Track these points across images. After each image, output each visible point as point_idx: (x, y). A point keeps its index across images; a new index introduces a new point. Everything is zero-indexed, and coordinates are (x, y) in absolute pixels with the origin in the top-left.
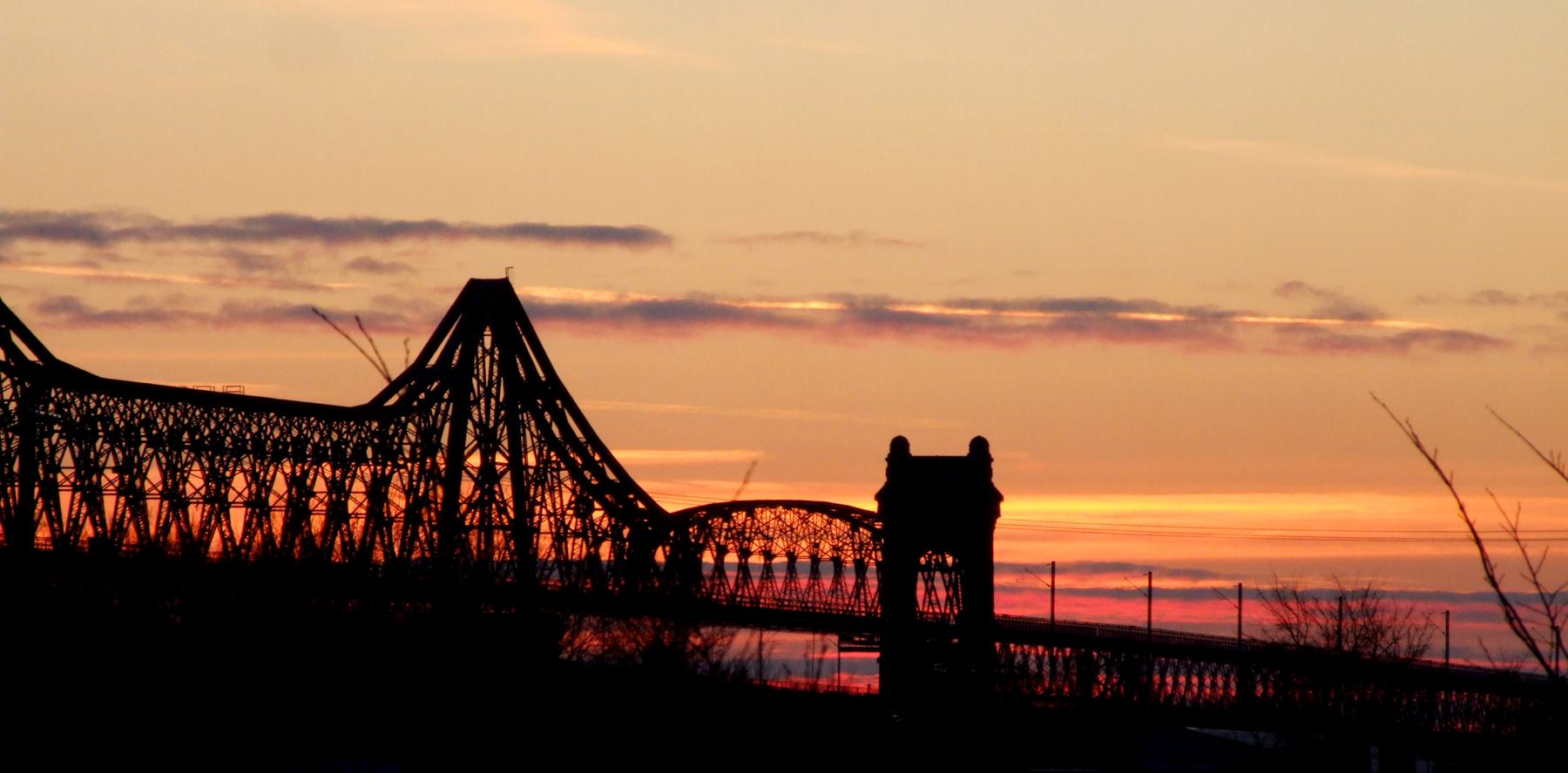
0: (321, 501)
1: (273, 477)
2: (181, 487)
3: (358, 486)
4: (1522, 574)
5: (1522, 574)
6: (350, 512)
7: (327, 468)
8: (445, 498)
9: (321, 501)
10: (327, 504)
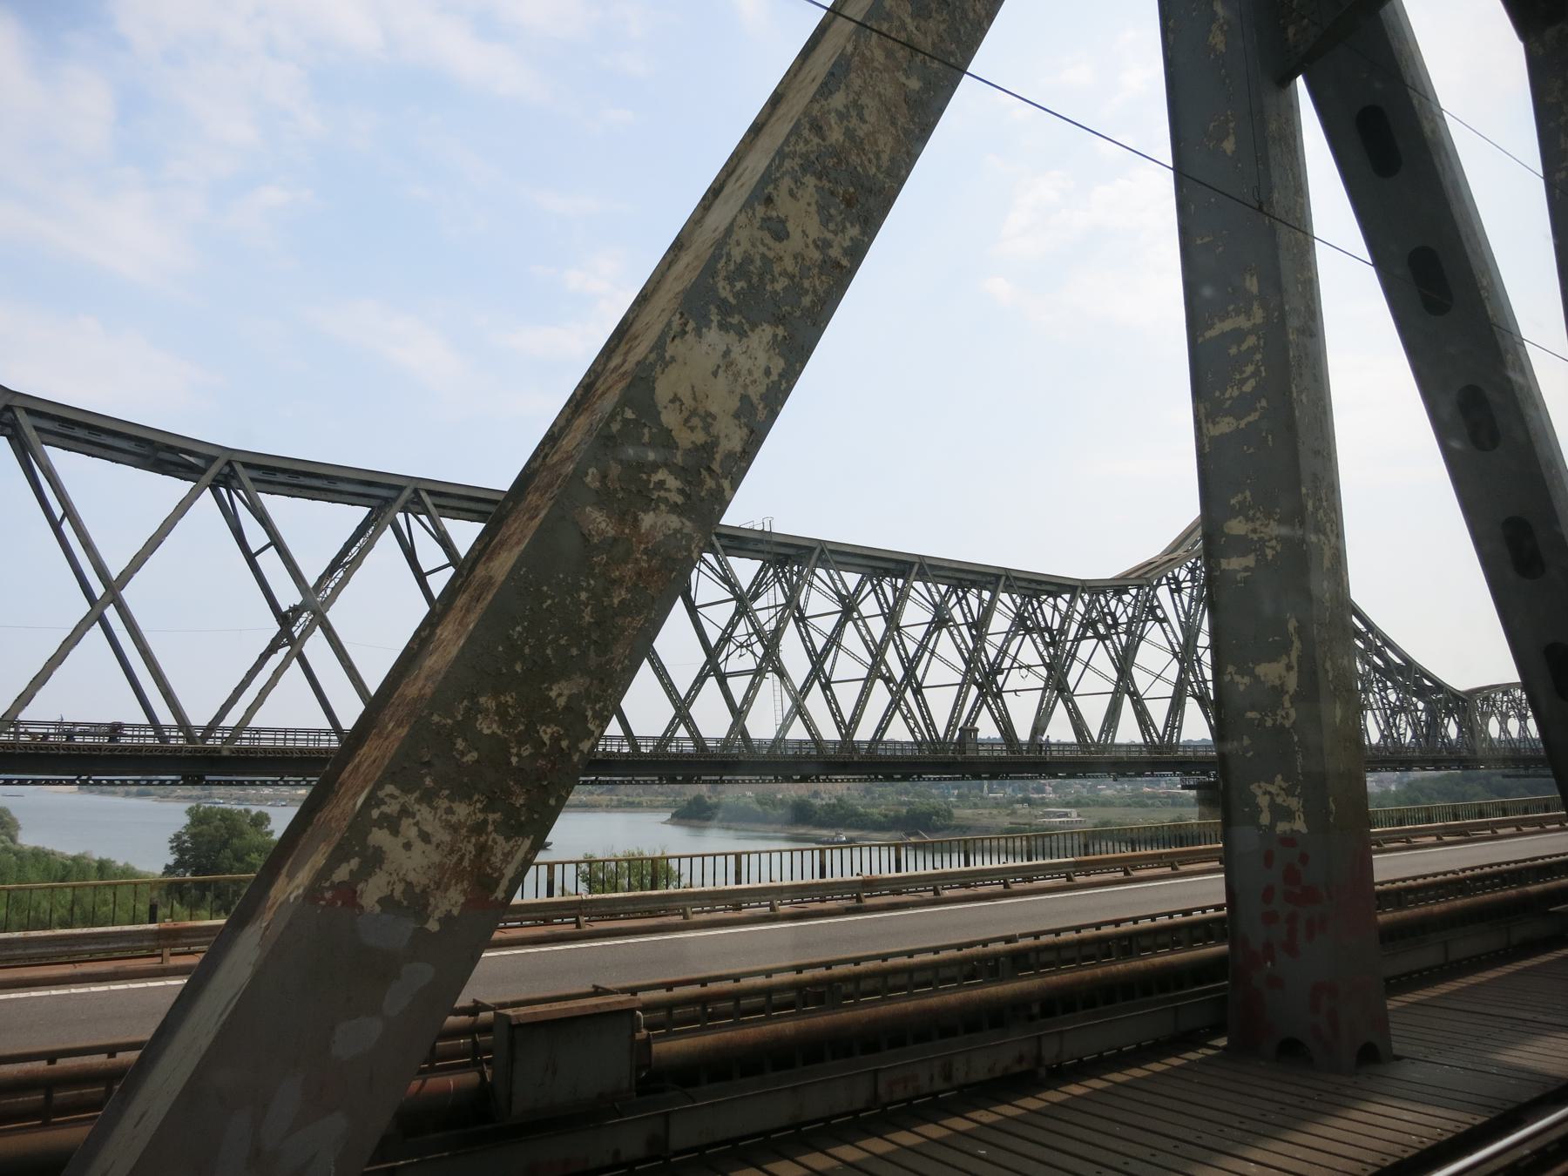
6: (1209, 650)
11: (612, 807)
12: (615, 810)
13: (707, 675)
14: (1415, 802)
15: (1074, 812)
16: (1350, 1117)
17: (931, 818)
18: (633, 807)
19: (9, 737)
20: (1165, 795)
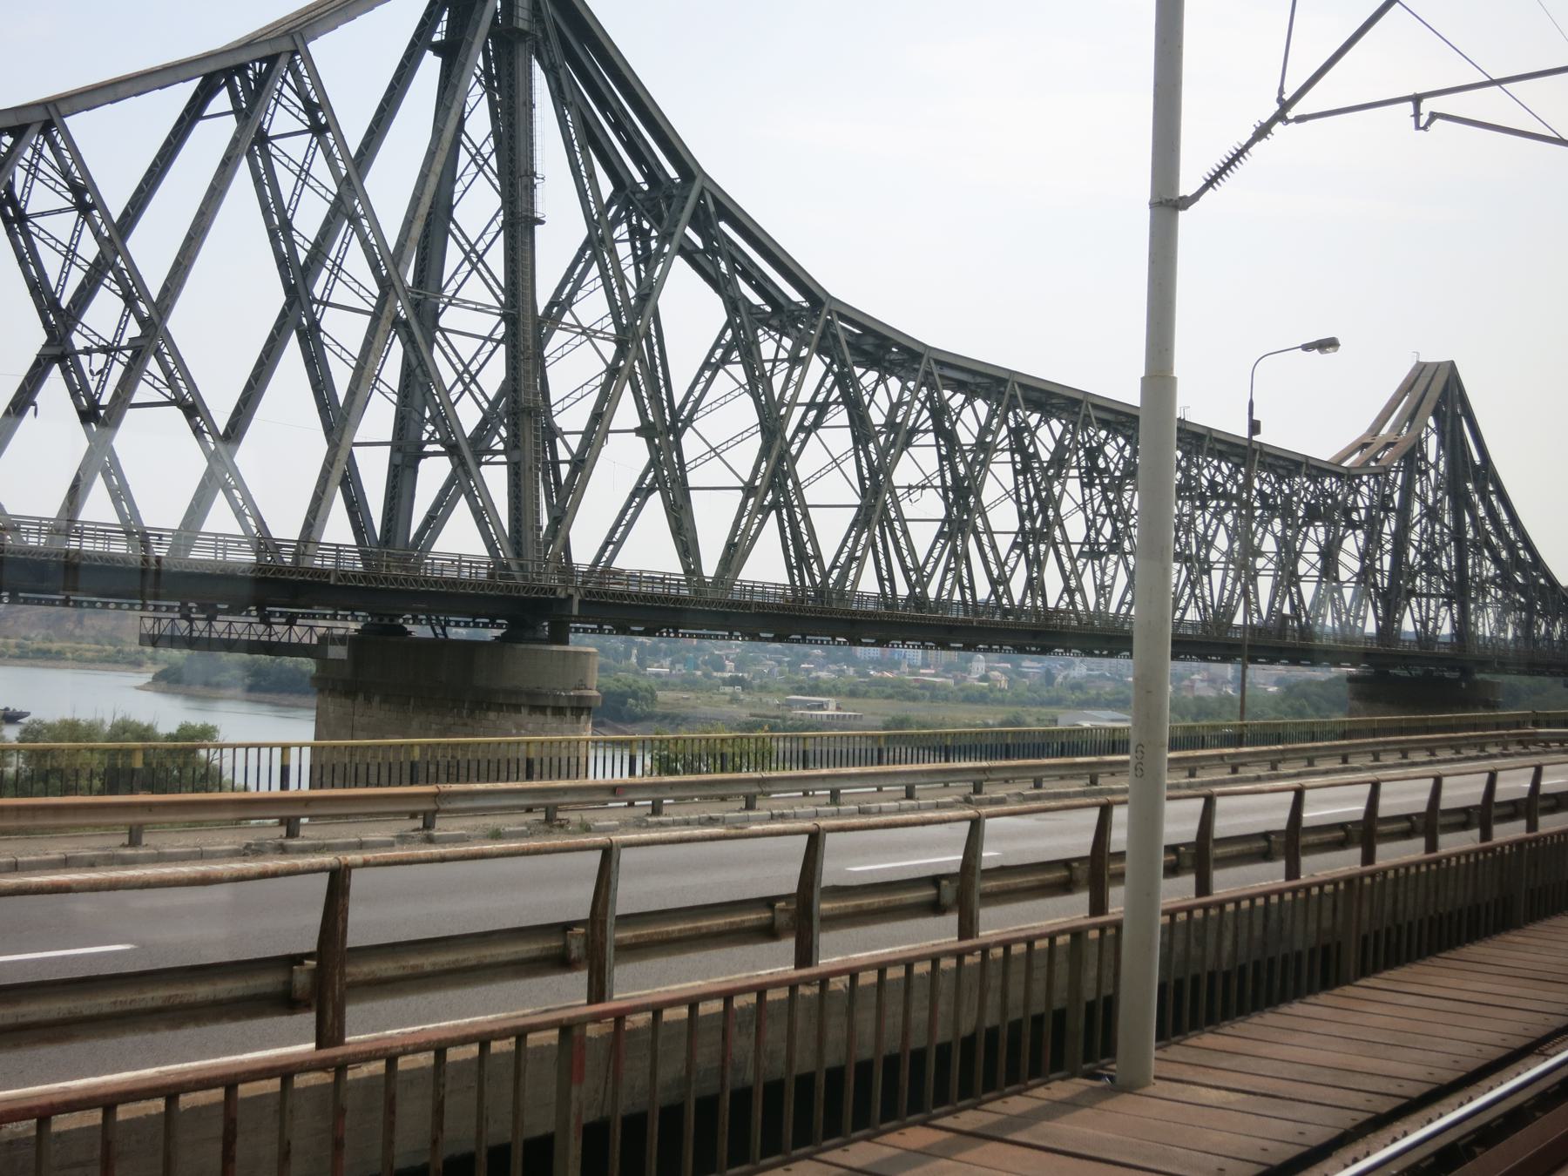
0: (1271, 560)
1: (1216, 532)
2: (1236, 545)
3: (1310, 547)
4: (36, 414)
5: (36, 414)
6: (502, 347)
7: (1277, 524)
8: (620, 318)
9: (1271, 560)
10: (1276, 564)
11: (10, 656)
12: (17, 662)
13: (651, 490)
14: (1300, 713)
15: (832, 702)
16: (883, 1142)
17: (625, 703)
18: (48, 659)
19: (39, 538)
20: (918, 685)
